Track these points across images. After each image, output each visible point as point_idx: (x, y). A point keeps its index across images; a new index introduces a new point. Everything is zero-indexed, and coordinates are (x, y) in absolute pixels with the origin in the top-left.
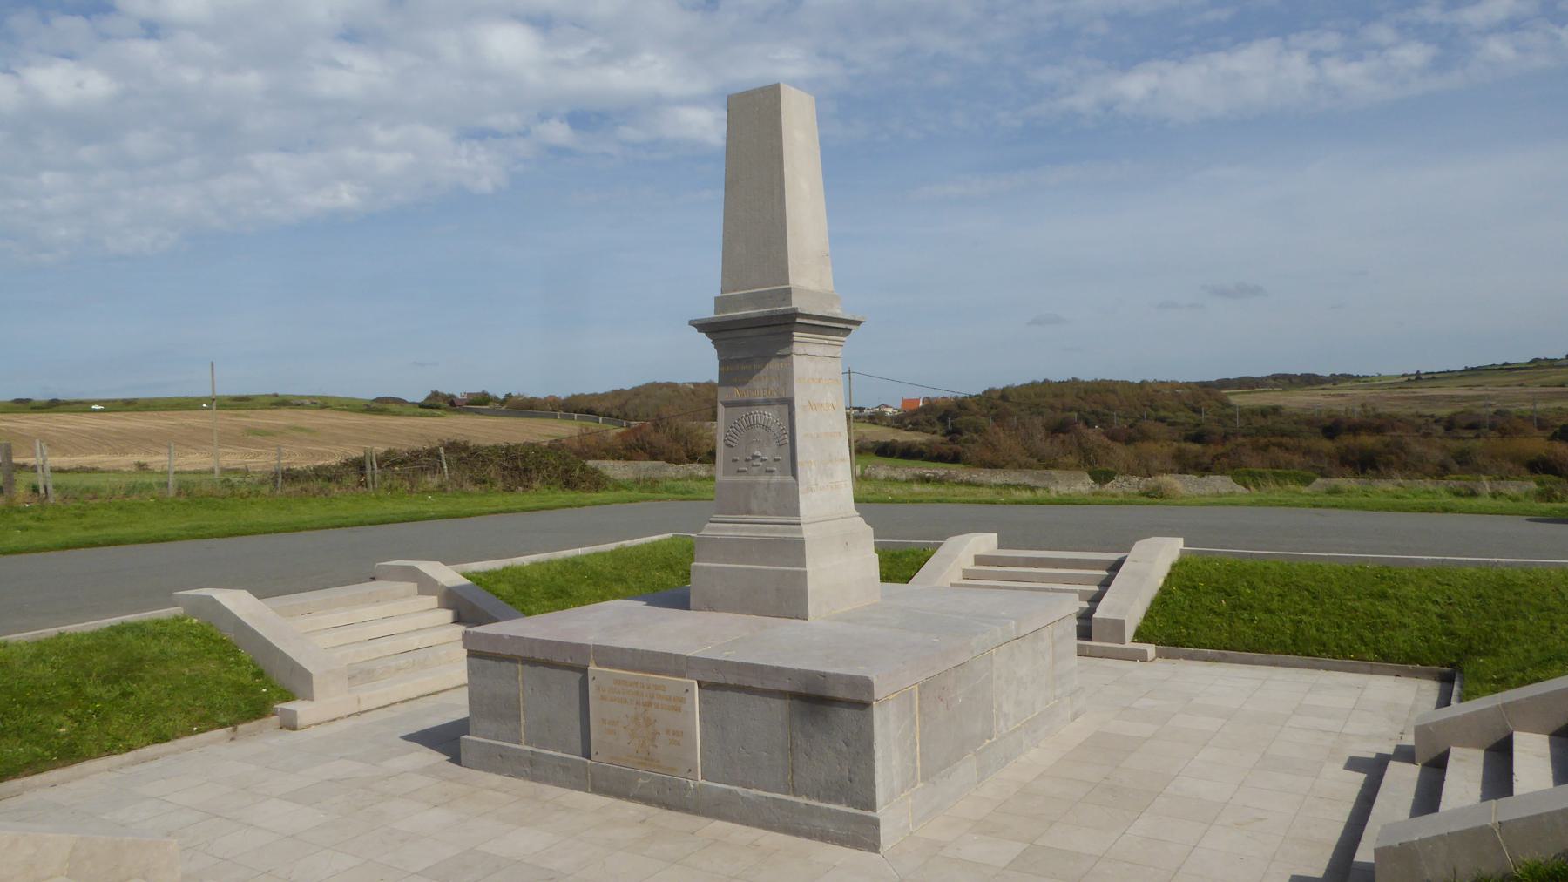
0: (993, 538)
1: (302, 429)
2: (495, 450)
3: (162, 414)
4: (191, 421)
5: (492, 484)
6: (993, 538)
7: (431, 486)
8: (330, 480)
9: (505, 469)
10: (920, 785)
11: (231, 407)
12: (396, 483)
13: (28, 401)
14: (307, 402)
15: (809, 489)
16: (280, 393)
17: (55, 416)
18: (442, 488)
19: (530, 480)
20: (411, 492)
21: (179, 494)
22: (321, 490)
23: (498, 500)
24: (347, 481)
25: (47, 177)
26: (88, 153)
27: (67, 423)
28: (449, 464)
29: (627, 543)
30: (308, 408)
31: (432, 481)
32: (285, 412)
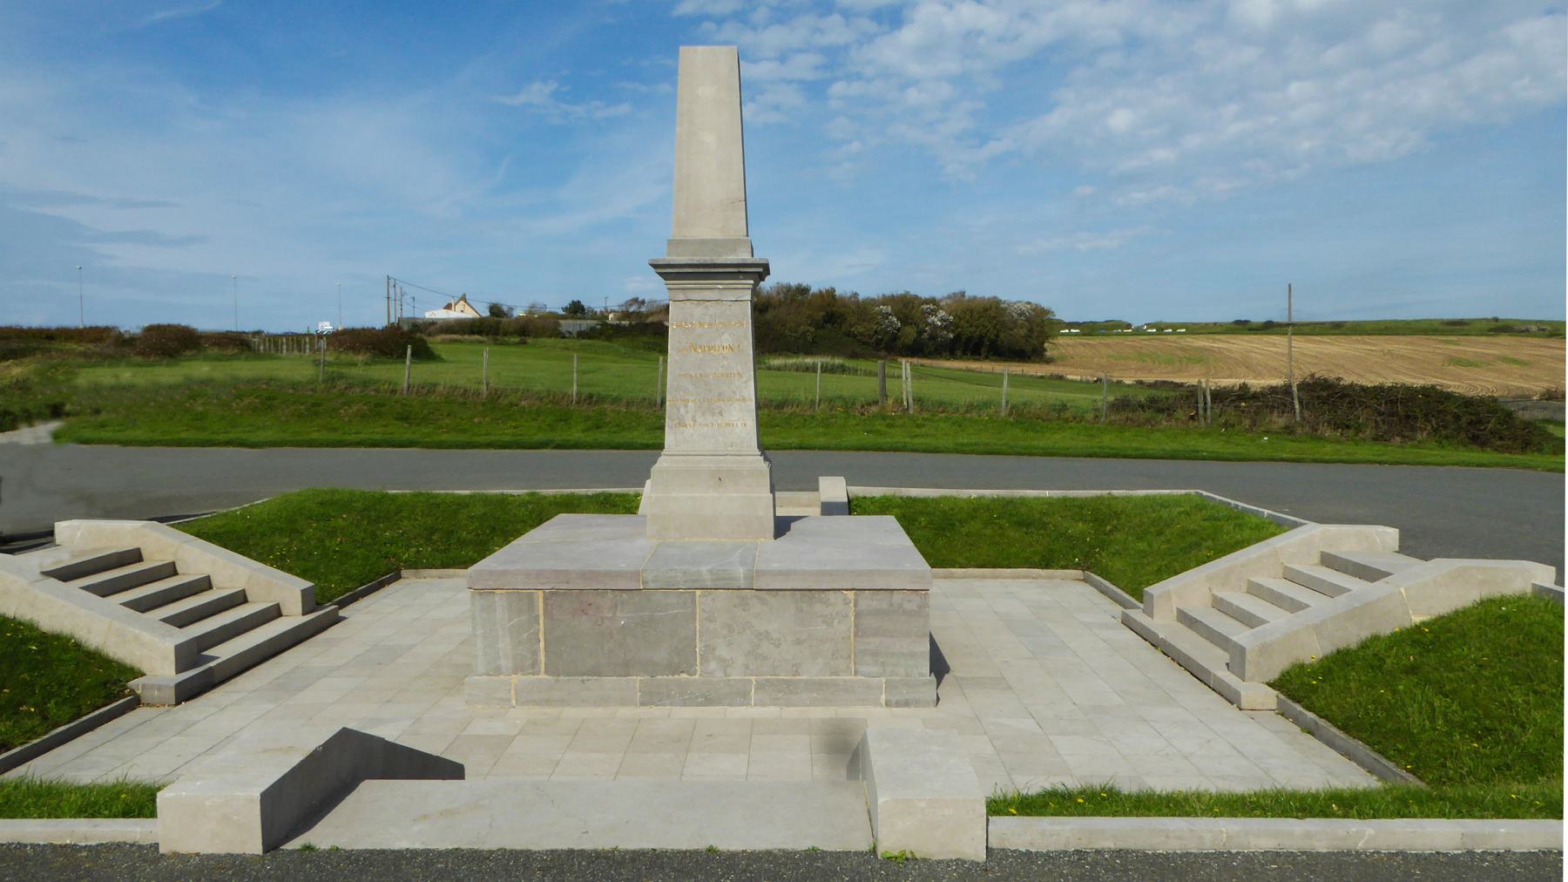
0: (1391, 535)
1: (1515, 361)
2: (1378, 391)
3: (1366, 338)
4: (1390, 347)
5: (1358, 430)
6: (1391, 535)
7: (1275, 427)
8: (1160, 411)
9: (1380, 414)
10: (543, 676)
11: (1443, 333)
12: (1233, 420)
13: (1246, 322)
14: (1534, 328)
15: (682, 424)
16: (1501, 317)
17: (1266, 338)
18: (1289, 430)
19: (1413, 429)
20: (1250, 430)
21: (1010, 414)
22: (1148, 421)
23: (1366, 451)
24: (1179, 414)
25: (1294, 88)
26: (1333, 56)
27: (1274, 345)
28: (1301, 403)
29: (1115, 492)
30: (1534, 335)
31: (1280, 421)
32: (1503, 339)
